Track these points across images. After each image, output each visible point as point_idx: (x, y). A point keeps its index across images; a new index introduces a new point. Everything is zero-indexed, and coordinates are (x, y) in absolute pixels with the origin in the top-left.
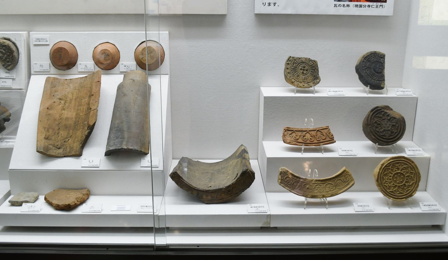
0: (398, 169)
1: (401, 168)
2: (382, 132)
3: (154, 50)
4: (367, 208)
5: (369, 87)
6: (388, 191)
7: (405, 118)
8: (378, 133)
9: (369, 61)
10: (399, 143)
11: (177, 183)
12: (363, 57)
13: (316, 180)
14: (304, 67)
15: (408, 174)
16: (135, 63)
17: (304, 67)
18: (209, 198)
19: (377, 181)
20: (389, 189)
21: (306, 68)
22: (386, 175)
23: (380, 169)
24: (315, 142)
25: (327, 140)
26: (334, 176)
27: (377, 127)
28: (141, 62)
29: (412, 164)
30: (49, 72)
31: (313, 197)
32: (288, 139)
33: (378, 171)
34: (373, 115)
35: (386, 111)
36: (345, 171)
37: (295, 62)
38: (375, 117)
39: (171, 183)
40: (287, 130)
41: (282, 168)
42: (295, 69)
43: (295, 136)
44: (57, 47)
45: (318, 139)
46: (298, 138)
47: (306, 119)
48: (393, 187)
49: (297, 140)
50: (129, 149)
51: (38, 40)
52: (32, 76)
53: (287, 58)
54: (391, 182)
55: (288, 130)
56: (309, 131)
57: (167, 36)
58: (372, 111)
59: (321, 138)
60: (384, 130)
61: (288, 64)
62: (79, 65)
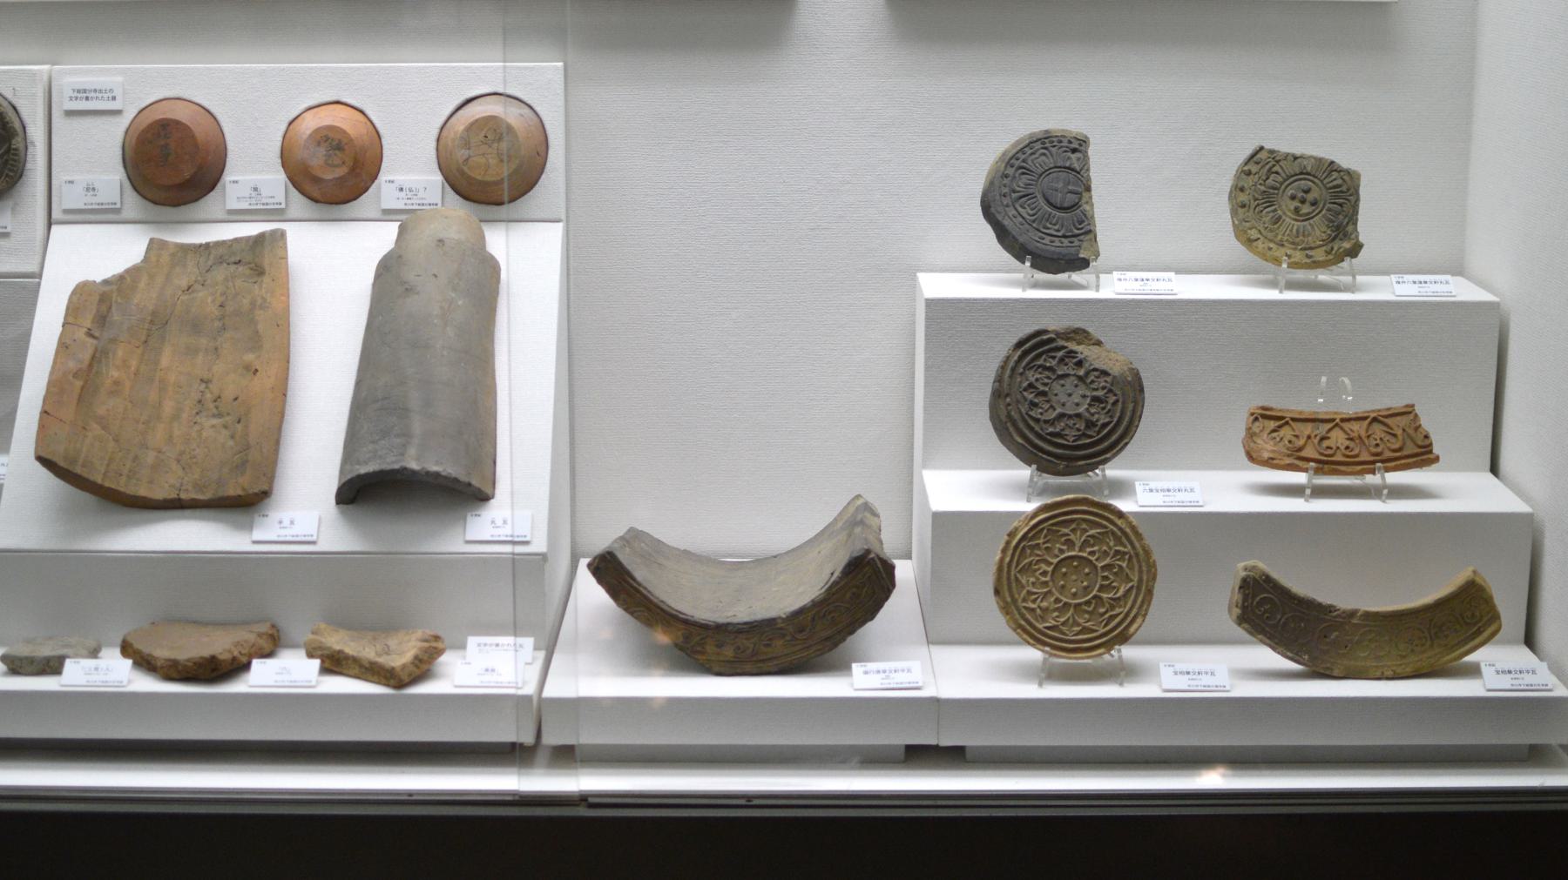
3: (510, 128)
4: (1206, 680)
5: (1028, 264)
6: (1040, 626)
7: (1142, 375)
8: (1037, 428)
9: (1025, 171)
11: (613, 592)
12: (1001, 159)
14: (1307, 191)
16: (439, 178)
17: (1307, 191)
18: (729, 652)
19: (997, 592)
20: (1043, 619)
21: (1310, 197)
22: (1025, 570)
23: (1004, 551)
24: (1365, 457)
25: (1405, 453)
27: (1035, 405)
28: (463, 173)
30: (118, 211)
32: (1267, 447)
33: (998, 557)
34: (1021, 358)
35: (1072, 346)
37: (1277, 168)
38: (1028, 367)
39: (590, 594)
40: (1263, 415)
42: (1267, 198)
44: (150, 121)
45: (1374, 450)
46: (1301, 442)
47: (1324, 379)
49: (1300, 449)
50: (428, 473)
51: (83, 94)
52: (54, 228)
53: (1249, 152)
54: (1050, 592)
56: (1343, 420)
57: (560, 78)
58: (1020, 344)
60: (1062, 416)
61: (1249, 173)
62: (229, 187)
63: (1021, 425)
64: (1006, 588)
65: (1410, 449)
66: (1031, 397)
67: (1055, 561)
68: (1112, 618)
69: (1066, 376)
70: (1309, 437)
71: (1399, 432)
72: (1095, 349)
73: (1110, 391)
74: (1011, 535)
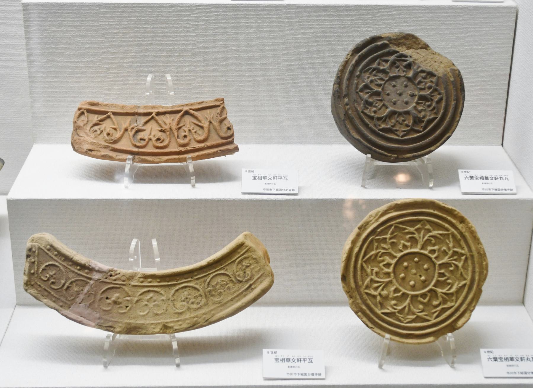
0: (414, 241)
1: (422, 237)
2: (384, 119)
4: (304, 368)
6: (379, 312)
7: (463, 74)
8: (371, 125)
10: (445, 149)
13: (146, 277)
15: (445, 260)
19: (344, 278)
20: (382, 305)
23: (354, 242)
24: (174, 148)
25: (208, 144)
26: (204, 263)
27: (371, 104)
29: (460, 226)
31: (130, 330)
32: (88, 138)
34: (358, 63)
36: (241, 246)
40: (94, 113)
41: (37, 235)
43: (108, 130)
45: (181, 141)
46: (118, 135)
48: (395, 298)
49: (115, 142)
54: (390, 282)
55: (89, 111)
56: (158, 114)
58: (357, 50)
59: (196, 139)
60: (393, 114)
63: (358, 122)
64: (352, 275)
65: (215, 140)
66: (366, 96)
67: (399, 255)
68: (444, 310)
69: (398, 77)
70: (126, 130)
71: (206, 124)
72: (423, 52)
73: (435, 90)
74: (362, 228)
